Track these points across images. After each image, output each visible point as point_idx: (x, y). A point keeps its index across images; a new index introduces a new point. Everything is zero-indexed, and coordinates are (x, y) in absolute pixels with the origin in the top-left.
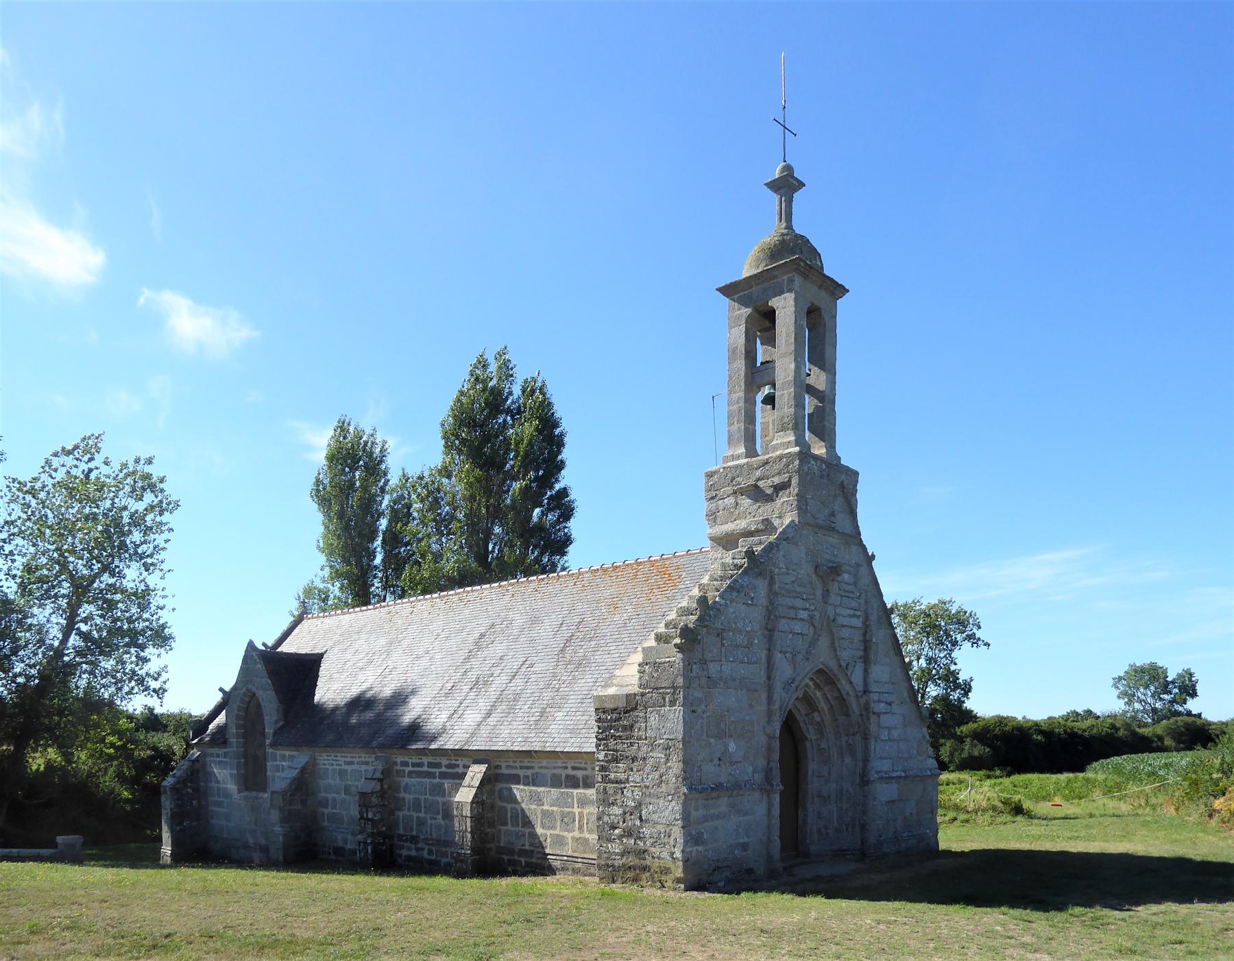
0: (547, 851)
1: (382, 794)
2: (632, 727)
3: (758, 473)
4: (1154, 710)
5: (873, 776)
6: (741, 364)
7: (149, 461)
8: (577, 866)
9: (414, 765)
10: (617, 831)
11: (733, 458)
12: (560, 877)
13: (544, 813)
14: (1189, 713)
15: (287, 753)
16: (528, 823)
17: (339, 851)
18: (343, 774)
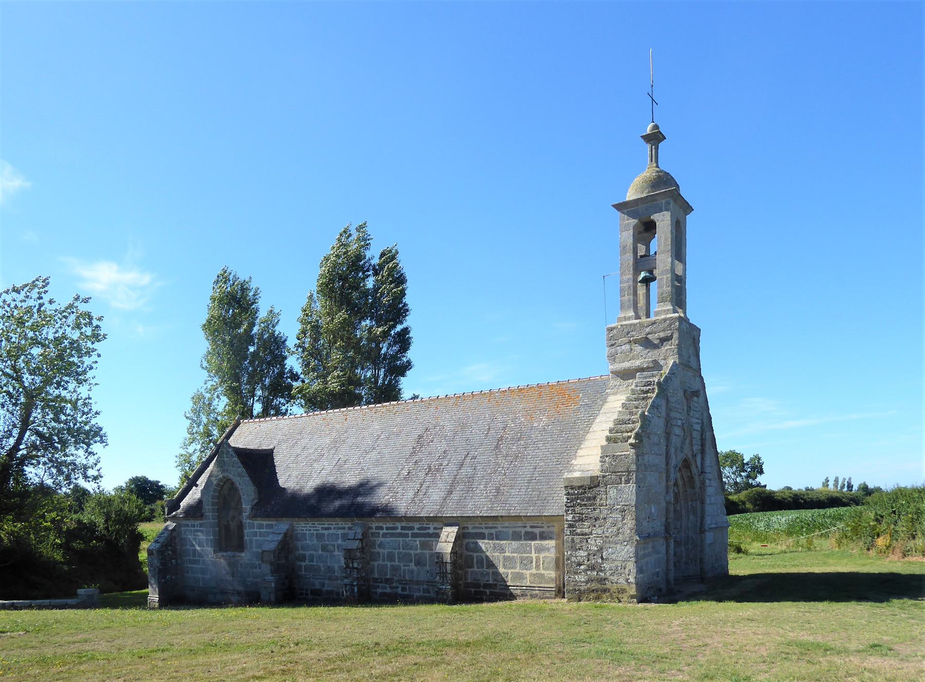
0: (508, 584)
1: (362, 550)
2: (594, 498)
3: (648, 330)
4: (736, 483)
5: (706, 527)
6: (630, 257)
7: (86, 301)
8: (534, 592)
9: (387, 529)
10: (582, 567)
11: (625, 319)
12: (519, 602)
13: (505, 558)
14: (759, 485)
15: (265, 523)
16: (491, 565)
18: (320, 537)
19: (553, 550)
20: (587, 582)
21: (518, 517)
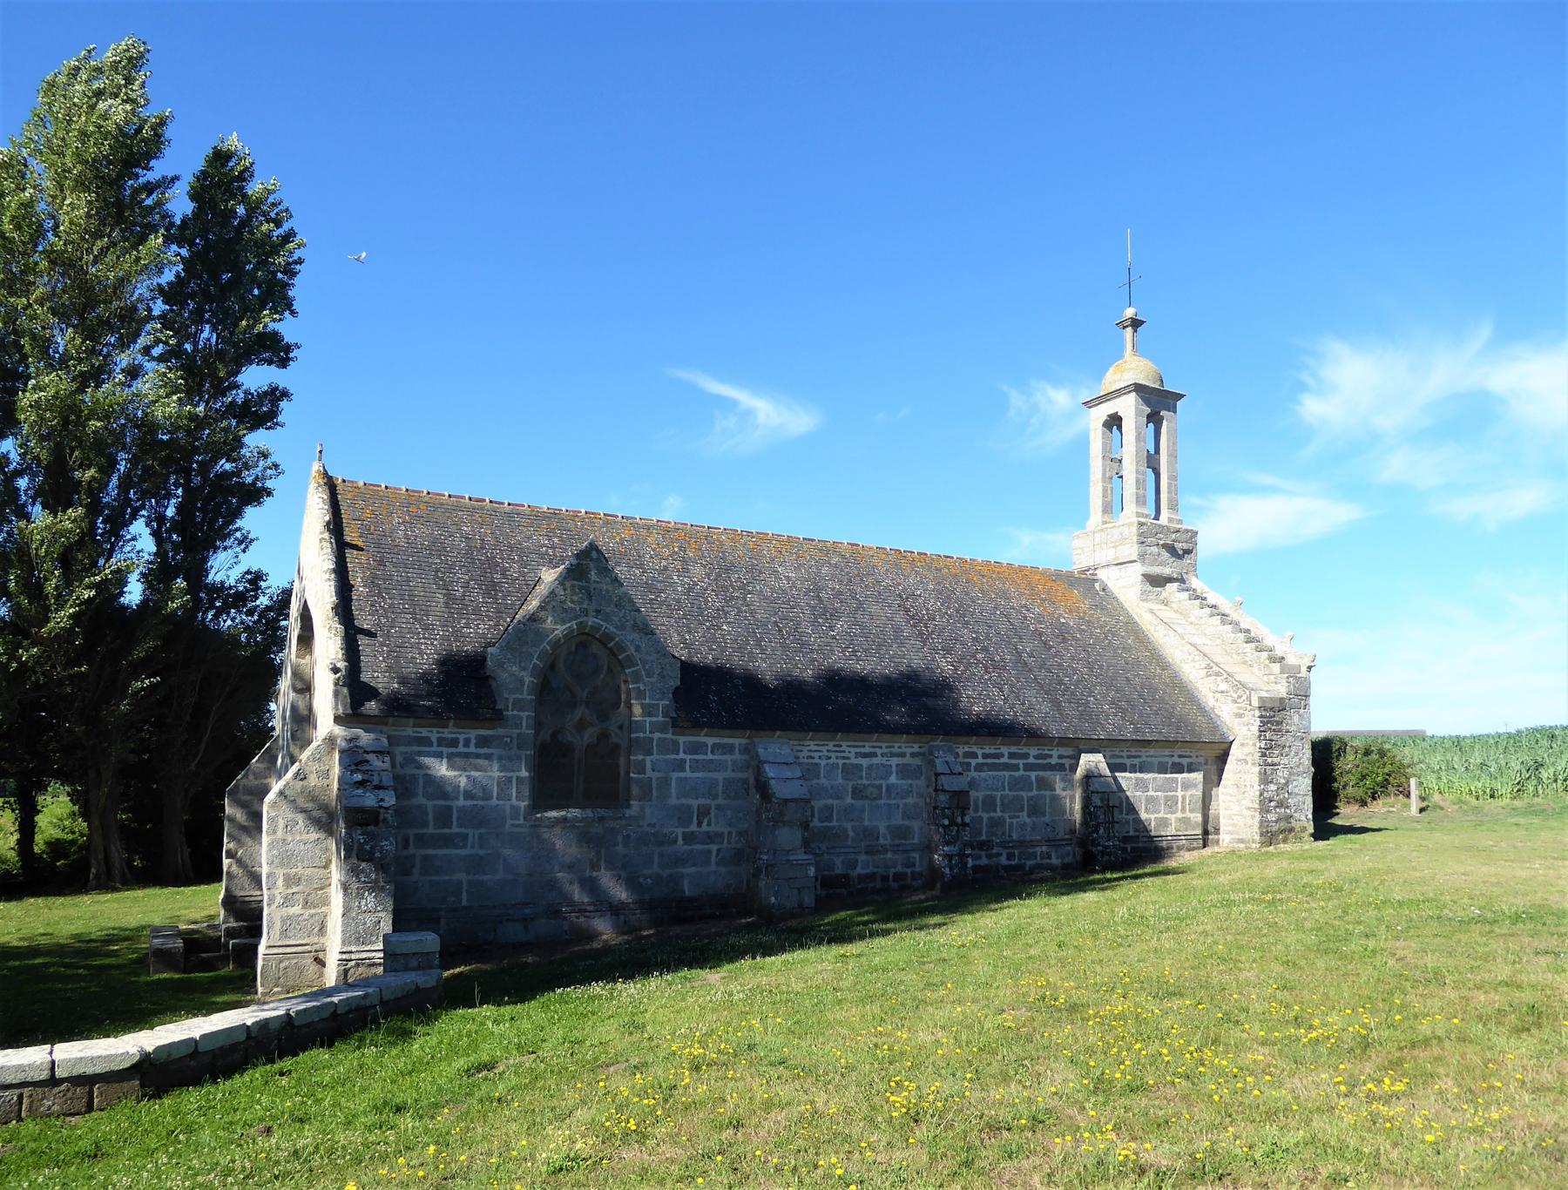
9: (985, 756)
15: (710, 741)
16: (1132, 809)
18: (850, 771)
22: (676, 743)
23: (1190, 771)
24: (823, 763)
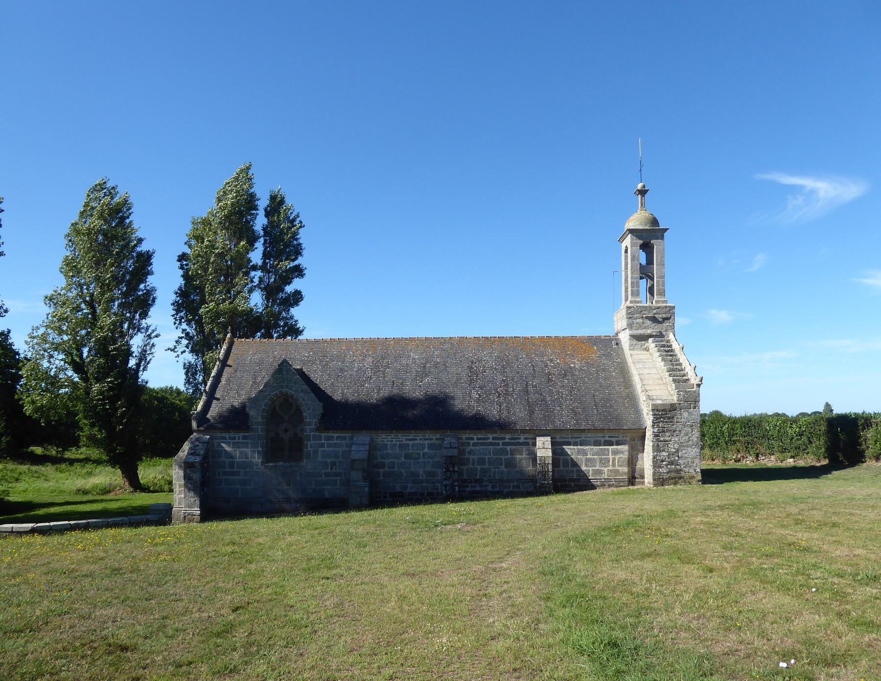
9: (478, 439)
13: (587, 460)
15: (335, 435)
16: (575, 464)
17: (532, 480)
18: (402, 447)
19: (626, 453)
20: (668, 473)
21: (602, 430)
22: (320, 437)
23: (618, 444)
24: (389, 443)
